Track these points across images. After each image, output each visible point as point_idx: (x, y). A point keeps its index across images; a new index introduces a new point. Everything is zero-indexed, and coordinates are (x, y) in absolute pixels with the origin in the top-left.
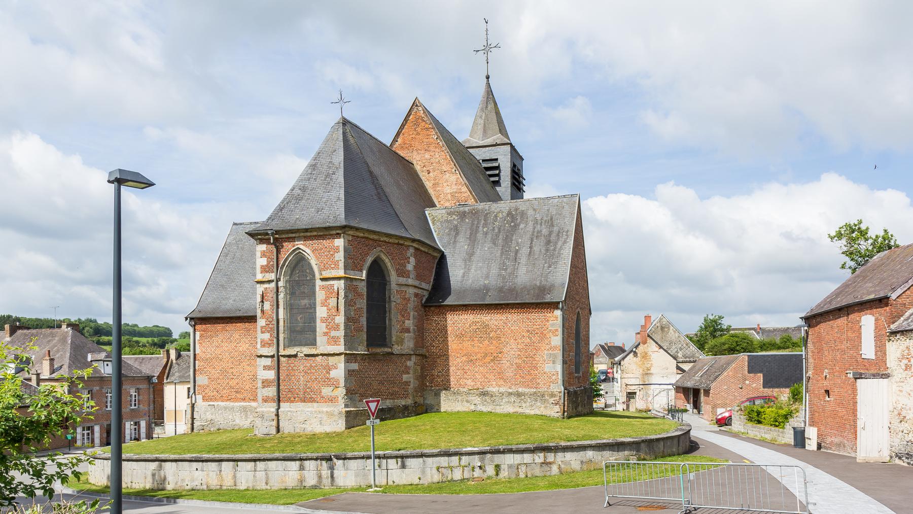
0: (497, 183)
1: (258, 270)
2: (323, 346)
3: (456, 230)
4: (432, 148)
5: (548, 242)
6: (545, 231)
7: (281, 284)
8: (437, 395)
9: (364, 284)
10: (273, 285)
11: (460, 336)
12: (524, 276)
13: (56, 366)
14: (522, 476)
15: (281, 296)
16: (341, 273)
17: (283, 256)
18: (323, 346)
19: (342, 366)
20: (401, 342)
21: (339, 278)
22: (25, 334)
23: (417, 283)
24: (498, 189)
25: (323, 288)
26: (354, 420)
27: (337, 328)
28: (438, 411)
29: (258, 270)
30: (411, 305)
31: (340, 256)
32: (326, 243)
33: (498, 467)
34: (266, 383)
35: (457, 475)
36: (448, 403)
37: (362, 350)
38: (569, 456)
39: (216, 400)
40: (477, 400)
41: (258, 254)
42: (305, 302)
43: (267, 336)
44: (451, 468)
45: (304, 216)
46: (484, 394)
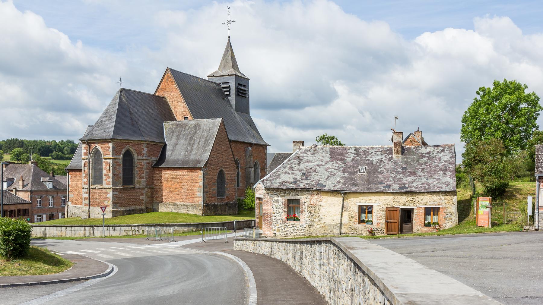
0: (229, 95)
1: (83, 154)
2: (105, 185)
3: (173, 132)
4: (174, 91)
5: (206, 140)
6: (206, 135)
7: (90, 160)
8: (158, 205)
9: (122, 160)
10: (88, 160)
11: (166, 180)
12: (193, 156)
13: (25, 184)
14: (151, 234)
15: (91, 165)
16: (111, 157)
17: (91, 149)
18: (105, 185)
19: (111, 193)
20: (139, 183)
21: (110, 159)
22: (13, 167)
23: (149, 158)
24: (229, 98)
25: (105, 162)
26: (115, 214)
27: (109, 178)
28: (158, 211)
29: (83, 154)
30: (144, 168)
31: (110, 150)
32: (106, 145)
33: (143, 231)
34: (85, 199)
35: (131, 233)
36: (162, 209)
37: (120, 187)
38: (168, 228)
39: (76, 204)
40: (172, 207)
41: (83, 148)
42: (99, 167)
43: (86, 180)
44: (129, 231)
45: (99, 134)
46: (175, 205)
